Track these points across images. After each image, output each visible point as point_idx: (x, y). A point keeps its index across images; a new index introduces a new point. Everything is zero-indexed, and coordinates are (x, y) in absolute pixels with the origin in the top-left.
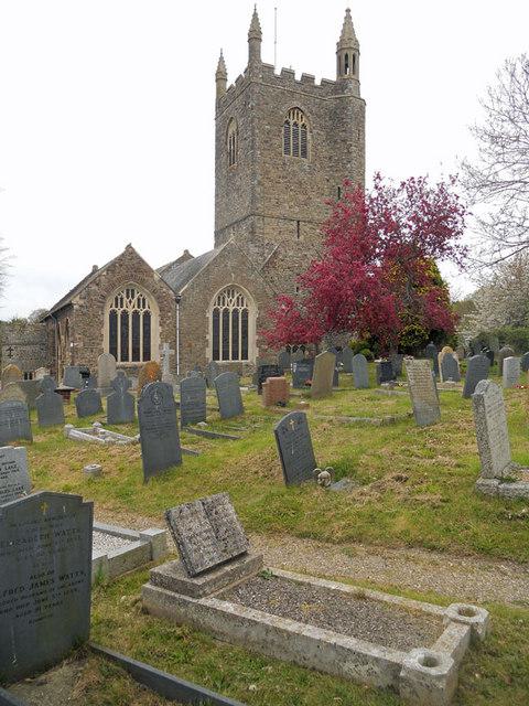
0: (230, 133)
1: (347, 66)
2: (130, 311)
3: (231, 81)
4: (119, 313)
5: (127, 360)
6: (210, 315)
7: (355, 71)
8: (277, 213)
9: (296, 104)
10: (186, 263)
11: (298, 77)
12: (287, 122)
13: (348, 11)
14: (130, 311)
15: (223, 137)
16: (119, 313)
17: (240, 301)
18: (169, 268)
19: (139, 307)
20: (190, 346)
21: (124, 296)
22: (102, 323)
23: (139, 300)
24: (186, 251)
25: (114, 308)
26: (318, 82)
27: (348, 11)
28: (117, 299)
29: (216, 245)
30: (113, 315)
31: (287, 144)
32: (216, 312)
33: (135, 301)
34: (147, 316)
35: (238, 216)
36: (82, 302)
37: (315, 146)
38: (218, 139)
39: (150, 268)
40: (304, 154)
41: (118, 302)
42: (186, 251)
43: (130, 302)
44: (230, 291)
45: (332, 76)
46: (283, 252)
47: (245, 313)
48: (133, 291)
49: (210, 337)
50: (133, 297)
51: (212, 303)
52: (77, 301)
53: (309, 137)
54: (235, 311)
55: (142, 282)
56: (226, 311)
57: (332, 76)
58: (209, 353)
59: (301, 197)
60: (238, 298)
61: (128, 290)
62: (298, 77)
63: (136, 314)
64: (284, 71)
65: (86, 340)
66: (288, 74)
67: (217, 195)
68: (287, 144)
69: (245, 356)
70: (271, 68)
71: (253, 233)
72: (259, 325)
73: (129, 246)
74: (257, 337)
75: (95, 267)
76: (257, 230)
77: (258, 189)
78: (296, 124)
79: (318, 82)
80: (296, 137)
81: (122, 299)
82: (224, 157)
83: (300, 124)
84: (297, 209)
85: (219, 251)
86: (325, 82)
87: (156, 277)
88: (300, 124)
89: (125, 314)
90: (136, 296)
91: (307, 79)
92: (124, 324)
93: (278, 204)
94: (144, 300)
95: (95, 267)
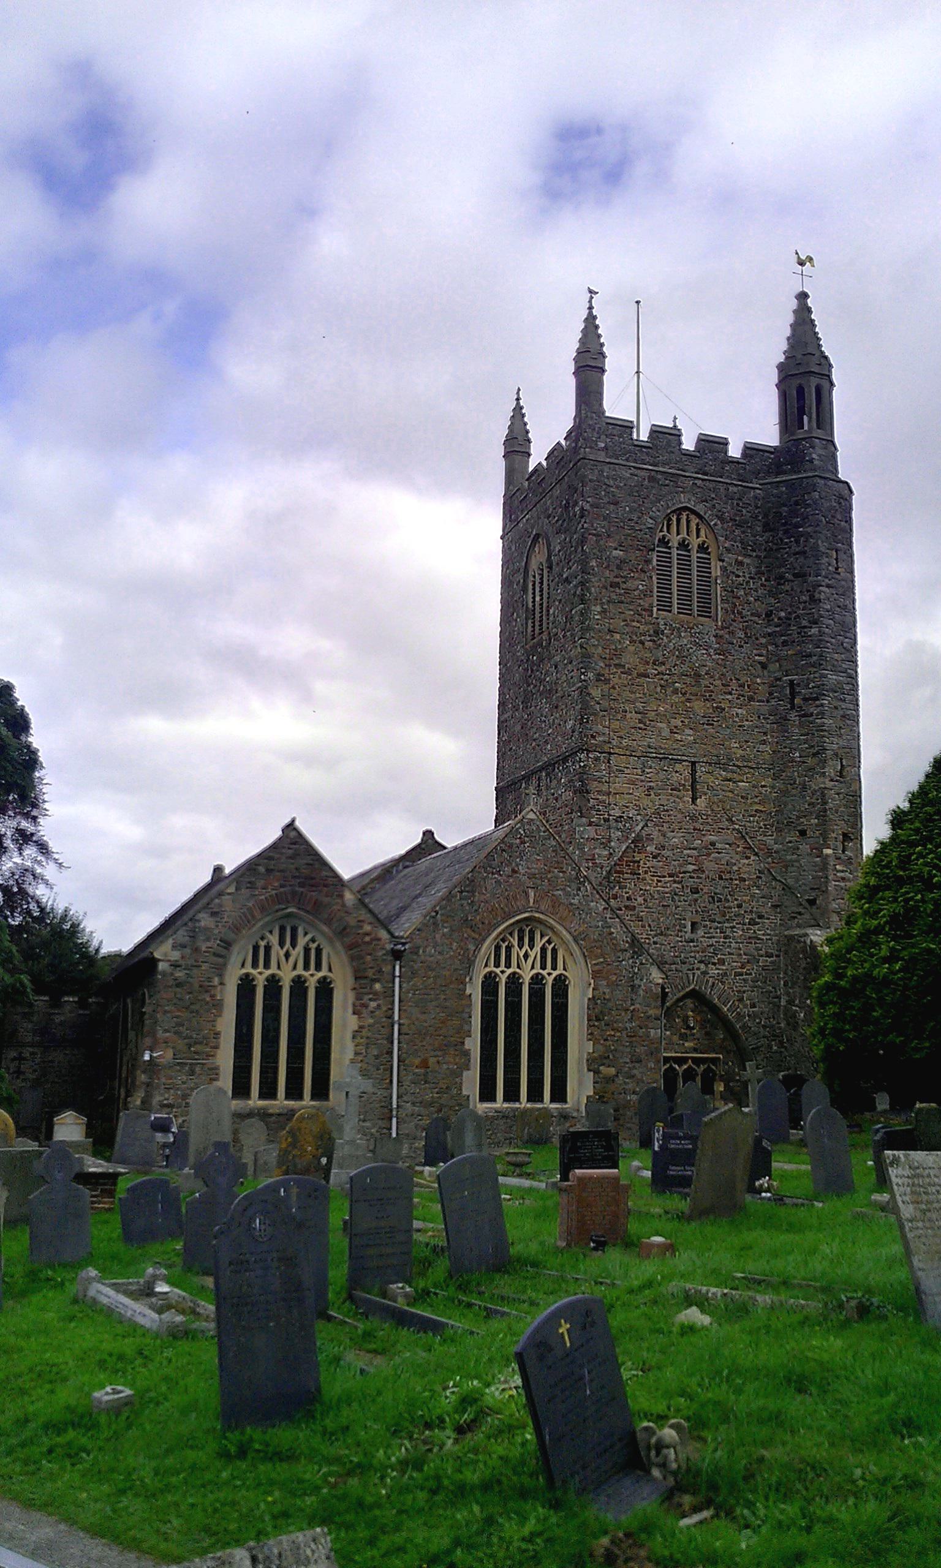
0: (534, 565)
1: (801, 411)
2: (287, 977)
3: (538, 456)
4: (312, 984)
5: (517, 1099)
6: (475, 991)
7: (824, 418)
8: (641, 742)
9: (684, 500)
10: (424, 863)
11: (689, 443)
12: (664, 542)
13: (803, 296)
14: (287, 977)
15: (520, 577)
16: (312, 984)
17: (313, 958)
18: (387, 872)
19: (306, 967)
20: (424, 1064)
21: (274, 939)
22: (219, 1005)
23: (307, 950)
24: (428, 834)
25: (300, 971)
26: (735, 451)
27: (803, 296)
28: (256, 949)
29: (498, 821)
30: (246, 987)
31: (665, 587)
32: (490, 985)
33: (298, 952)
34: (325, 990)
35: (550, 751)
36: (175, 955)
37: (730, 591)
38: (507, 582)
39: (336, 876)
40: (706, 609)
41: (260, 955)
42: (428, 834)
43: (287, 955)
44: (526, 930)
45: (769, 435)
46: (655, 834)
47: (561, 987)
48: (294, 931)
49: (474, 1044)
50: (294, 945)
51: (480, 962)
52: (164, 952)
53: (716, 570)
54: (537, 980)
55: (317, 909)
56: (514, 981)
57: (769, 435)
58: (471, 1082)
59: (699, 707)
60: (543, 950)
61: (282, 929)
62: (689, 443)
63: (299, 985)
64: (657, 432)
65: (181, 1044)
66: (665, 437)
67: (502, 705)
68: (665, 587)
69: (559, 1094)
70: (627, 427)
71: (583, 791)
72: (597, 1015)
73: (291, 826)
74: (590, 1047)
75: (218, 870)
76: (594, 786)
77: (596, 693)
78: (683, 545)
79: (735, 451)
80: (684, 572)
81: (268, 949)
82: (520, 617)
83: (695, 542)
84: (689, 736)
85: (500, 834)
86: (750, 450)
87: (349, 896)
88: (695, 542)
89: (273, 984)
90: (302, 941)
91: (712, 446)
92: (514, 1008)
93: (644, 723)
94: (319, 951)
95: (218, 870)
